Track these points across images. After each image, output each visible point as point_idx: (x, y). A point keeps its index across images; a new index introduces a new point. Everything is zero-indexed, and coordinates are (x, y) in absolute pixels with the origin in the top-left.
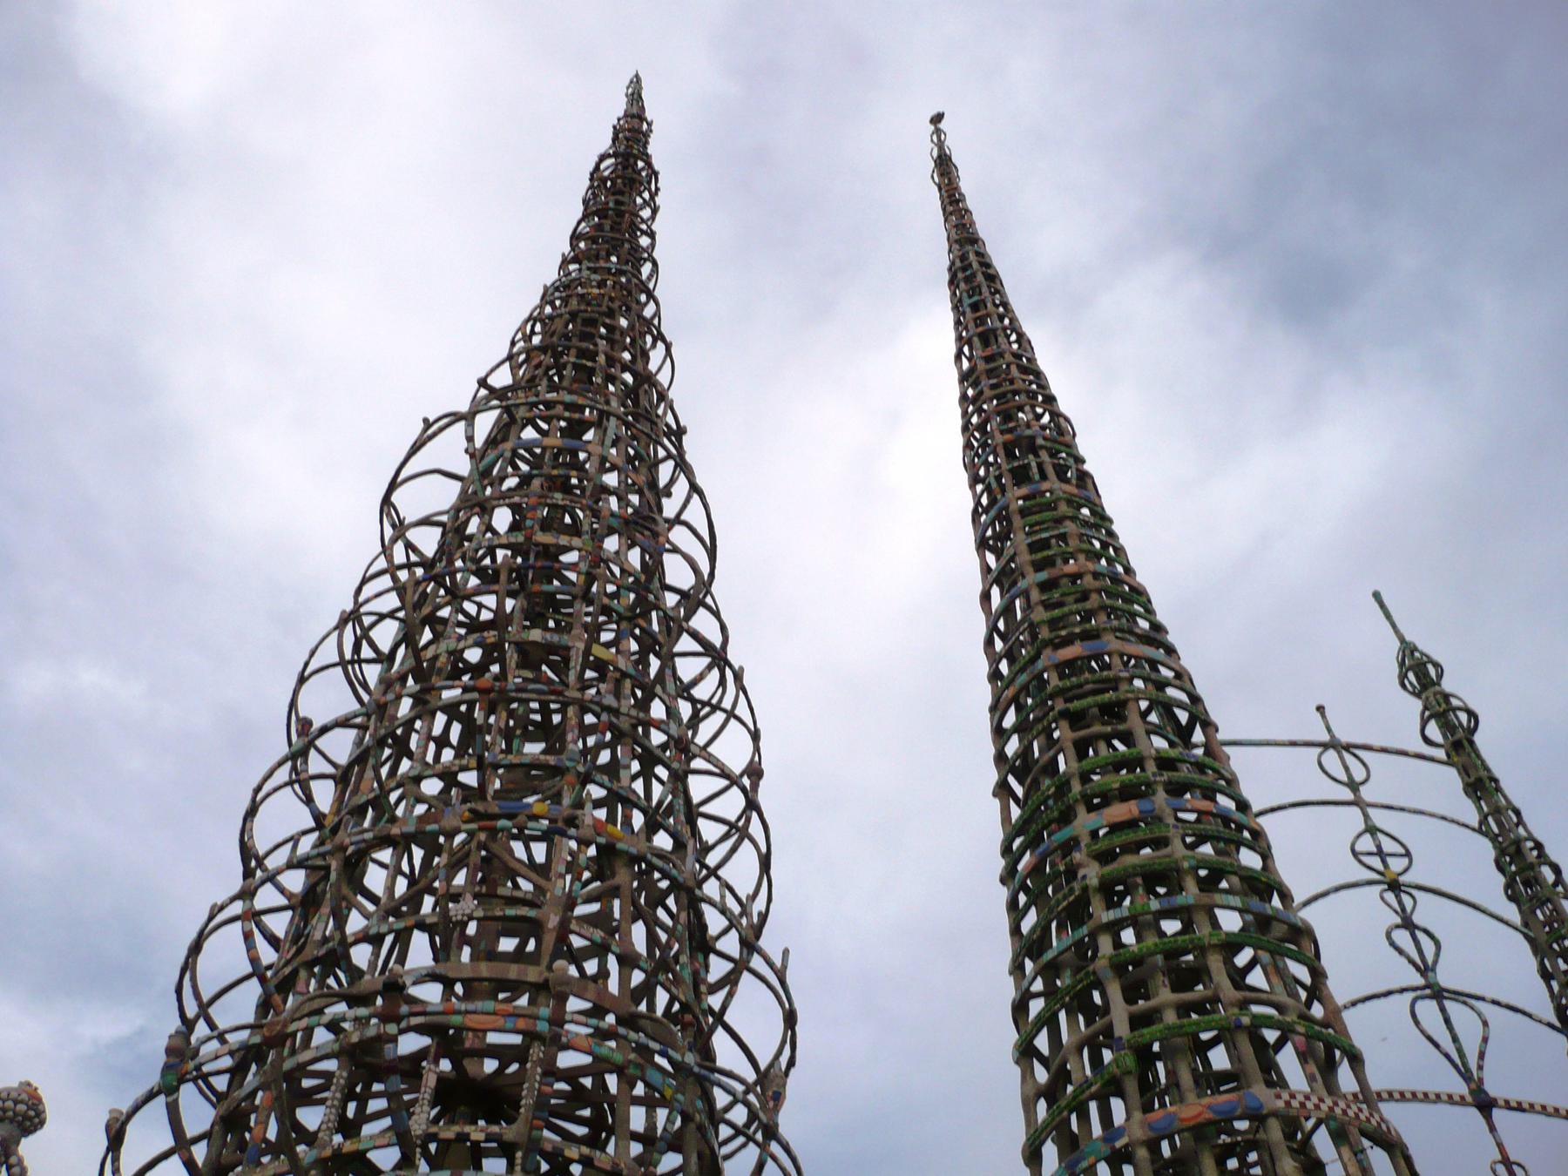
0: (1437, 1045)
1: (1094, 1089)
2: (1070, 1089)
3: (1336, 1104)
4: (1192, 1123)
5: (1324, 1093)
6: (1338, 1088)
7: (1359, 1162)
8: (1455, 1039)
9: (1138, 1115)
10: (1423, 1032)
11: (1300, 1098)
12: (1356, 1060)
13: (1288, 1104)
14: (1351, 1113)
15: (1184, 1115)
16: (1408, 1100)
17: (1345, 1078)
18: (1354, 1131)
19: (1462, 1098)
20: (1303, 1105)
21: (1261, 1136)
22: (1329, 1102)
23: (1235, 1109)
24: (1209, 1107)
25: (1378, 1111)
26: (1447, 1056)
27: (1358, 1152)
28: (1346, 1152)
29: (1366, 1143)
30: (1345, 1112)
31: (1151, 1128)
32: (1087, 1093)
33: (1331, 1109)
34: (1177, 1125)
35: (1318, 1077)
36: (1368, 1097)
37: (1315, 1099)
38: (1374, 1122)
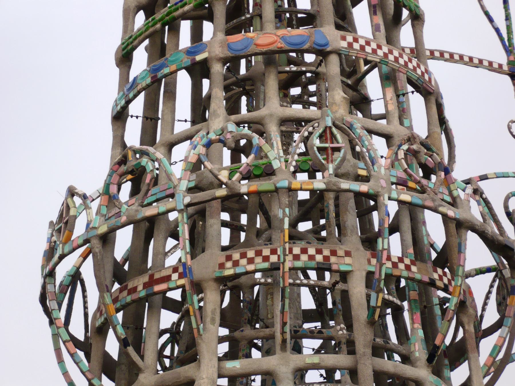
0: (491, 20)
1: (186, 8)
2: (169, 5)
3: (391, 52)
4: (265, 49)
5: (383, 42)
6: (399, 41)
7: (399, 104)
8: (508, 18)
9: (221, 36)
10: (483, 7)
11: (362, 42)
12: (417, 18)
13: (350, 45)
14: (401, 61)
15: (259, 42)
16: (456, 62)
17: (406, 35)
18: (402, 78)
19: (500, 66)
20: (362, 48)
21: (322, 69)
22: (385, 49)
23: (303, 43)
24: (283, 38)
25: (426, 65)
26: (497, 30)
27: (400, 95)
28: (390, 93)
29: (410, 89)
30: (396, 59)
31: (229, 47)
32: (180, 11)
33: (386, 55)
34: (253, 49)
35: (382, 28)
36: (417, 52)
37: (374, 45)
38: (419, 72)
